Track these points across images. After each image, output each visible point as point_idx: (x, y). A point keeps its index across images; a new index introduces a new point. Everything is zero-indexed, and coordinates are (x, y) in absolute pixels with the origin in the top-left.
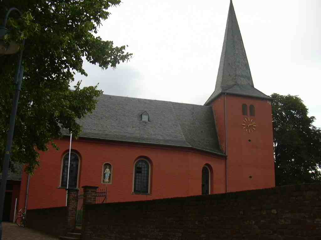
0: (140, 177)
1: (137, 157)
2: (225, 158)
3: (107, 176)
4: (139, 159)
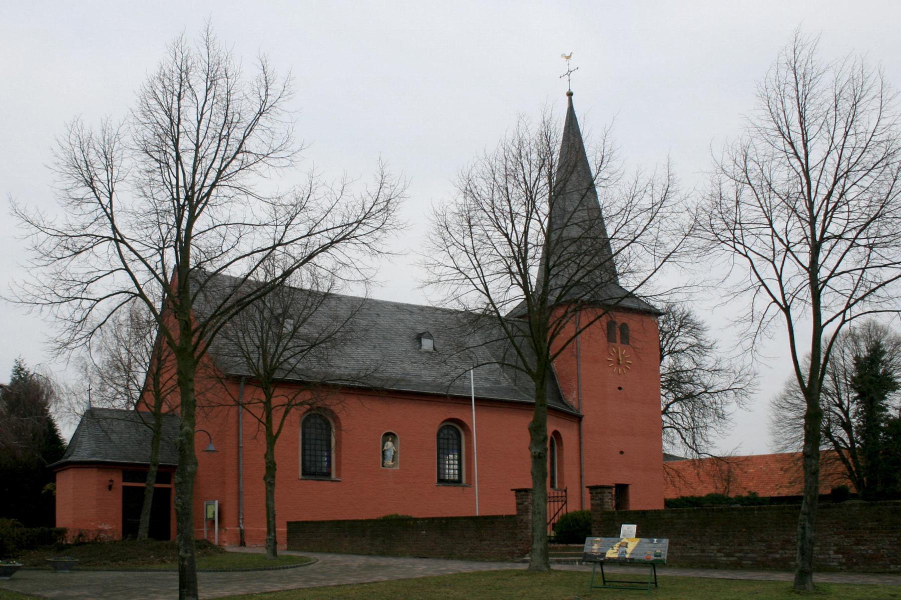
0: (313, 447)
1: (445, 418)
2: (579, 419)
3: (389, 454)
4: (448, 423)
